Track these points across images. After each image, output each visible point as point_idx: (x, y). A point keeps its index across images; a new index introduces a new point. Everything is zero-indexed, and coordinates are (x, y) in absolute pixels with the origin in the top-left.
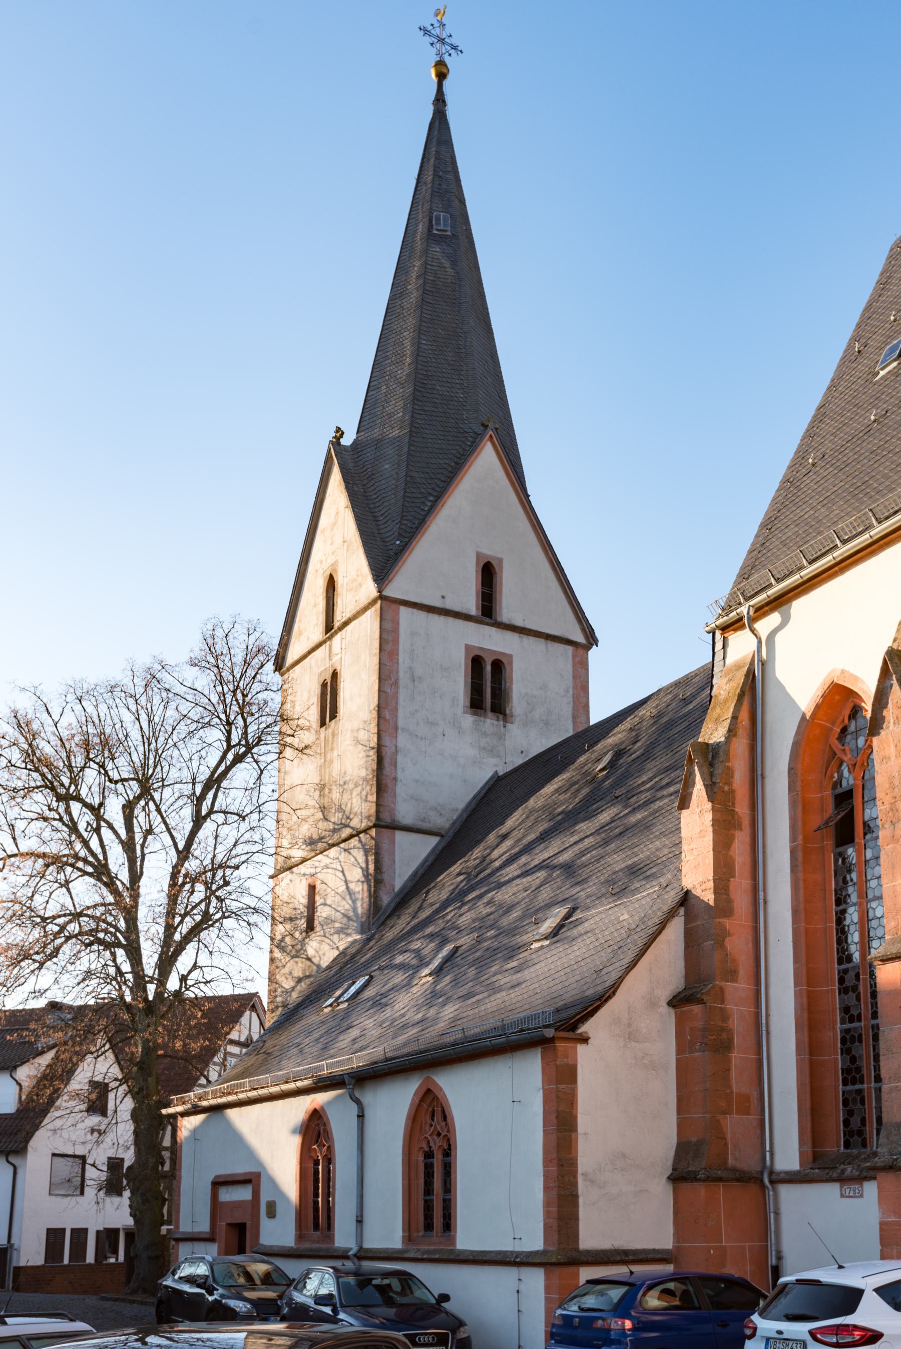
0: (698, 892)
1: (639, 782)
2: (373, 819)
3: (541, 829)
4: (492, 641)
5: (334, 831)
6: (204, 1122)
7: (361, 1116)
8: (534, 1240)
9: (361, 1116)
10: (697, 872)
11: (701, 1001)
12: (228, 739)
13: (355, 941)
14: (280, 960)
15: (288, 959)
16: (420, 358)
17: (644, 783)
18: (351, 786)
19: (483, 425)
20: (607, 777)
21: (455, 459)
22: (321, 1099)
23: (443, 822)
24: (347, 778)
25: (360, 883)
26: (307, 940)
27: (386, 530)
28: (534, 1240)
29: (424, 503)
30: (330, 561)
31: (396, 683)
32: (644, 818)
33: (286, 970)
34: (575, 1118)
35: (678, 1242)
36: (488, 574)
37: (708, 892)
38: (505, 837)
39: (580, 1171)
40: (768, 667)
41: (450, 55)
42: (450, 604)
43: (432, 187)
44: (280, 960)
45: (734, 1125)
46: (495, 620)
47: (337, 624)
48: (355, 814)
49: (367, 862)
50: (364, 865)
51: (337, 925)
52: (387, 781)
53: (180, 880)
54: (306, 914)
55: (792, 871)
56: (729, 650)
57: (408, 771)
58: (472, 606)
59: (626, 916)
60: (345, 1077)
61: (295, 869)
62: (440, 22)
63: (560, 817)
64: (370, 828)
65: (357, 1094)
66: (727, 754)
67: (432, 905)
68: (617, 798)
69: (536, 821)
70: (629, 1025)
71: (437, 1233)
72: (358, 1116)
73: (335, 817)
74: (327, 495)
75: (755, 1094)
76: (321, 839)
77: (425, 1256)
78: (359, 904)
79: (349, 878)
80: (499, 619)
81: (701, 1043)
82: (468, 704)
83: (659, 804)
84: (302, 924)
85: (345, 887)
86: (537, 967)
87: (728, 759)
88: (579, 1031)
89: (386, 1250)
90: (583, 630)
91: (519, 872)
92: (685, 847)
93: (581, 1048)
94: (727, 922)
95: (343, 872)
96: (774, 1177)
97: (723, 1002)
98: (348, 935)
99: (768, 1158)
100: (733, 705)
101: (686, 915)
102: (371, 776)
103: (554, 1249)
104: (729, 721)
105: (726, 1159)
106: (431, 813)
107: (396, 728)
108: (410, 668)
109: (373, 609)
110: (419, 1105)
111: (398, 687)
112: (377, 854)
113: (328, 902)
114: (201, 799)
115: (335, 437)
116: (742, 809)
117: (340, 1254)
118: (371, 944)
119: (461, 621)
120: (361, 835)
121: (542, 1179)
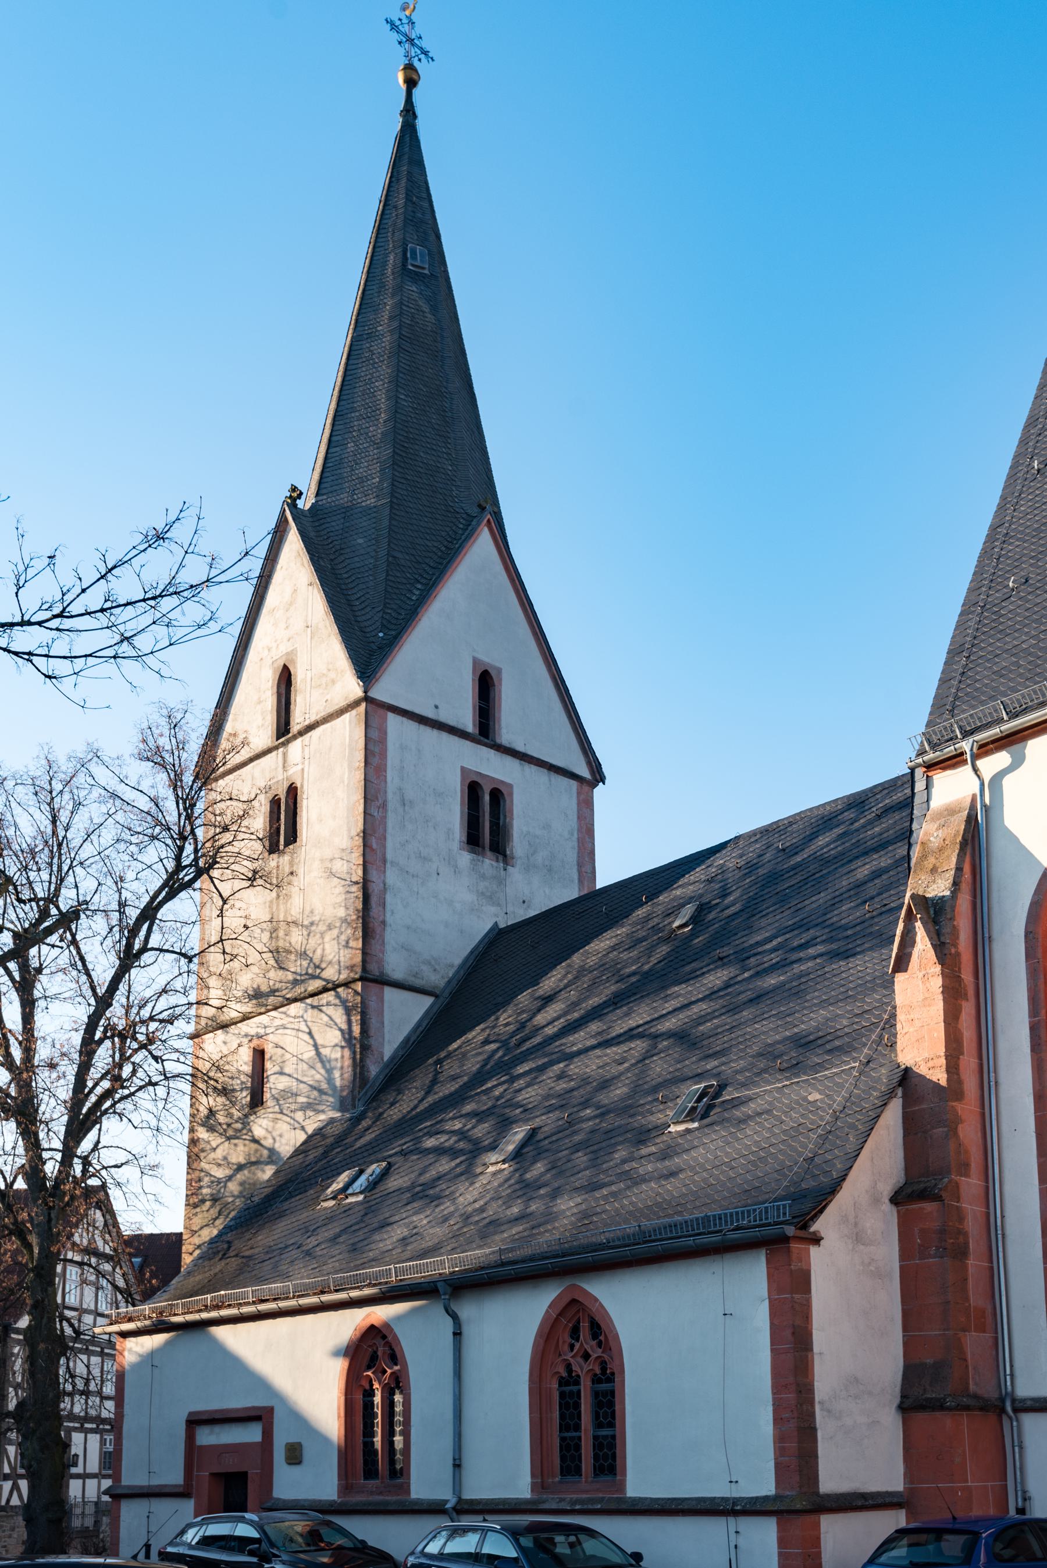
0: (923, 1070)
1: (752, 942)
2: (359, 970)
3: (608, 992)
4: (493, 767)
5: (295, 982)
6: (168, 1343)
7: (457, 1334)
8: (762, 1483)
9: (457, 1334)
10: (920, 1038)
11: (938, 1198)
12: (178, 858)
13: (332, 1121)
14: (208, 1142)
15: (219, 1140)
16: (398, 416)
17: (758, 944)
18: (322, 927)
19: (480, 506)
20: (693, 935)
21: (446, 543)
22: (382, 1313)
23: (437, 979)
24: (316, 918)
25: (339, 1049)
26: (252, 1118)
27: (364, 618)
28: (762, 1483)
29: (411, 591)
30: (284, 648)
31: (384, 806)
32: (783, 984)
33: (219, 1154)
34: (810, 1335)
35: (911, 1482)
36: (486, 684)
37: (938, 1070)
38: (548, 1000)
39: (817, 1399)
40: (993, 815)
41: (420, 60)
42: (444, 717)
43: (405, 213)
44: (208, 1142)
45: (973, 1342)
46: (494, 740)
47: (295, 728)
48: (330, 963)
49: (349, 1022)
50: (344, 1026)
51: (302, 1099)
52: (375, 924)
53: (98, 1035)
54: (249, 1085)
55: (1033, 1050)
56: (935, 791)
57: (398, 914)
58: (468, 721)
59: (818, 1096)
60: (439, 1285)
61: (233, 1029)
62: (409, 18)
63: (634, 979)
64: (354, 981)
65: (454, 1307)
66: (953, 908)
67: (454, 1078)
68: (721, 959)
69: (594, 983)
70: (856, 1224)
71: (586, 1478)
72: (455, 1334)
73: (296, 966)
74: (279, 567)
75: (989, 1310)
76: (273, 992)
77: (578, 1507)
78: (337, 1074)
79: (320, 1041)
80: (498, 741)
81: (938, 1248)
82: (465, 839)
83: (797, 968)
84: (244, 1097)
85: (314, 1053)
86: (693, 1153)
87: (952, 919)
88: (812, 1230)
89: (505, 1501)
90: (589, 763)
91: (593, 1042)
92: (901, 1017)
93: (814, 1250)
94: (959, 1106)
95: (310, 1033)
96: (1018, 1405)
97: (958, 1199)
98: (318, 1112)
99: (1009, 1383)
100: (955, 854)
101: (905, 1096)
102: (354, 917)
103: (794, 1493)
104: (953, 872)
105: (968, 1384)
106: (424, 968)
107: (384, 861)
108: (400, 789)
109: (354, 712)
110: (556, 1320)
111: (386, 811)
112: (363, 1014)
113: (287, 1070)
114: (134, 932)
115: (291, 497)
116: (967, 976)
117: (425, 1507)
118: (365, 1124)
119: (456, 738)
120: (339, 990)
121: (770, 1409)
